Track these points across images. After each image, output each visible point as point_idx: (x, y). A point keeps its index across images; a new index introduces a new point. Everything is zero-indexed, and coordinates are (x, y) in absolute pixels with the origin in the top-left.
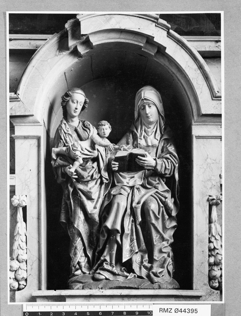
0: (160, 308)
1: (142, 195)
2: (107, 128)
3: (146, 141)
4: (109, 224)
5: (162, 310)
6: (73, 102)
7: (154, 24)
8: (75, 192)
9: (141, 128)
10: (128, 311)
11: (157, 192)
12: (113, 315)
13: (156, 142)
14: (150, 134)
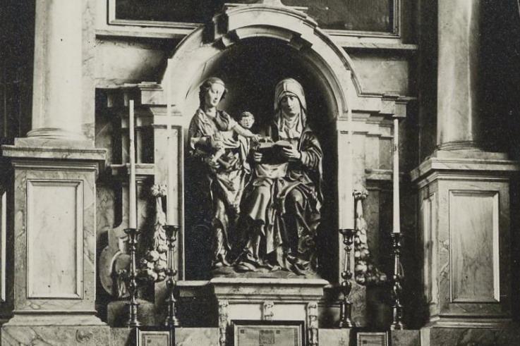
2: (249, 120)
3: (287, 133)
4: (253, 215)
6: (212, 91)
7: (302, 21)
9: (282, 121)
11: (301, 184)
13: (299, 135)
14: (291, 126)
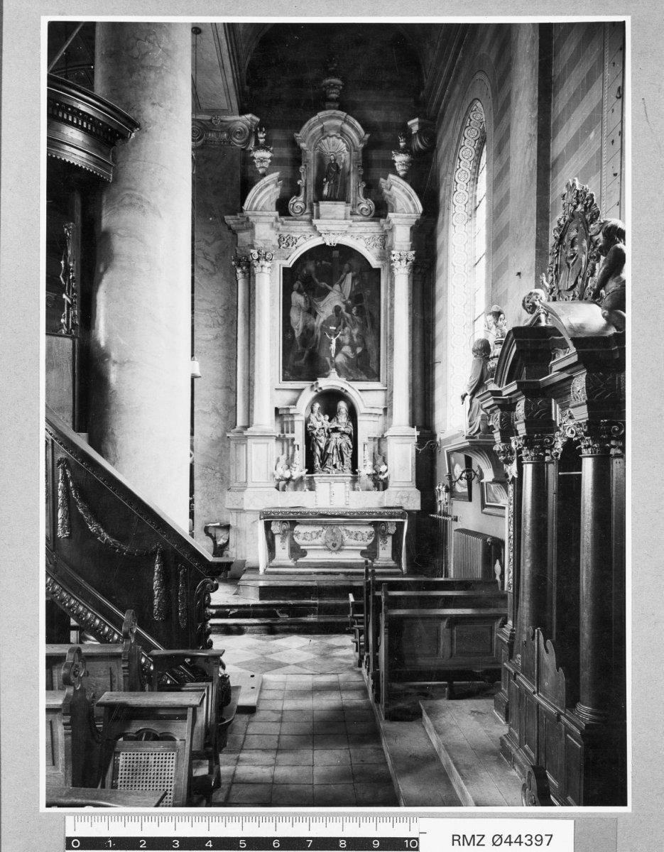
0: (453, 836)
1: (340, 441)
2: (327, 417)
4: (328, 451)
5: (457, 840)
8: (316, 439)
10: (351, 838)
12: (310, 849)
